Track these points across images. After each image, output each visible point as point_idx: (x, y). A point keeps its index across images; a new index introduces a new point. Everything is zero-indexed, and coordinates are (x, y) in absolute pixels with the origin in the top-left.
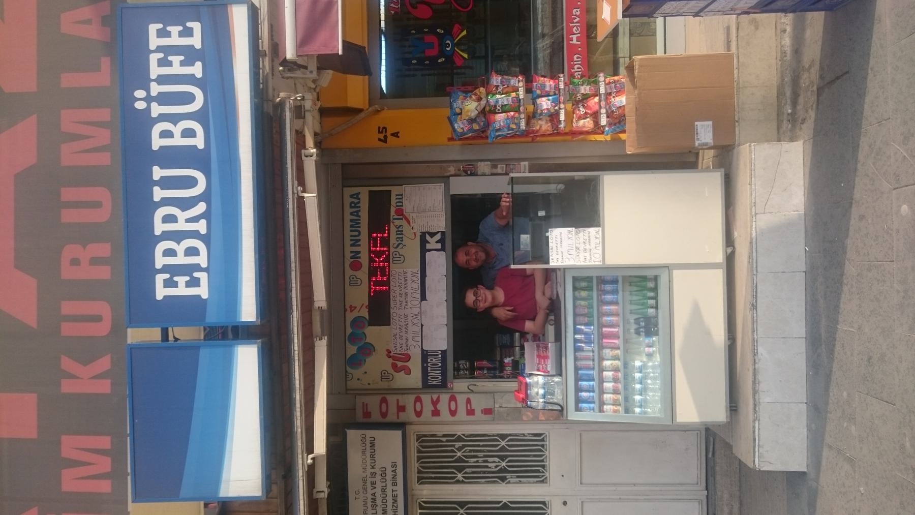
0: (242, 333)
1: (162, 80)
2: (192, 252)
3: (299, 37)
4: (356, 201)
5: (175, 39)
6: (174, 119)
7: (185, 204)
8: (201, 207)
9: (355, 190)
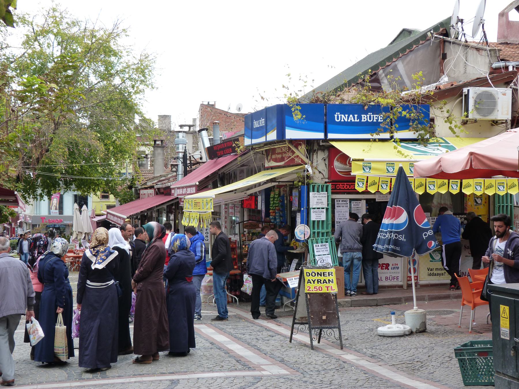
0: (326, 135)
1: (373, 117)
2: (364, 119)
3: (403, 173)
4: (322, 282)
6: (367, 118)
9: (334, 274)
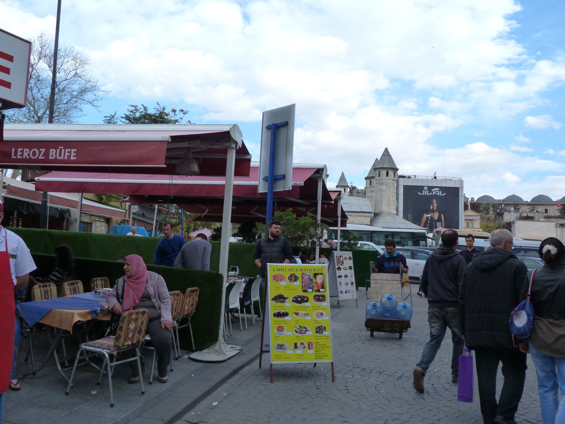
2: (52, 156)
5: (73, 154)
6: (56, 154)
7: (29, 155)
8: (28, 157)
